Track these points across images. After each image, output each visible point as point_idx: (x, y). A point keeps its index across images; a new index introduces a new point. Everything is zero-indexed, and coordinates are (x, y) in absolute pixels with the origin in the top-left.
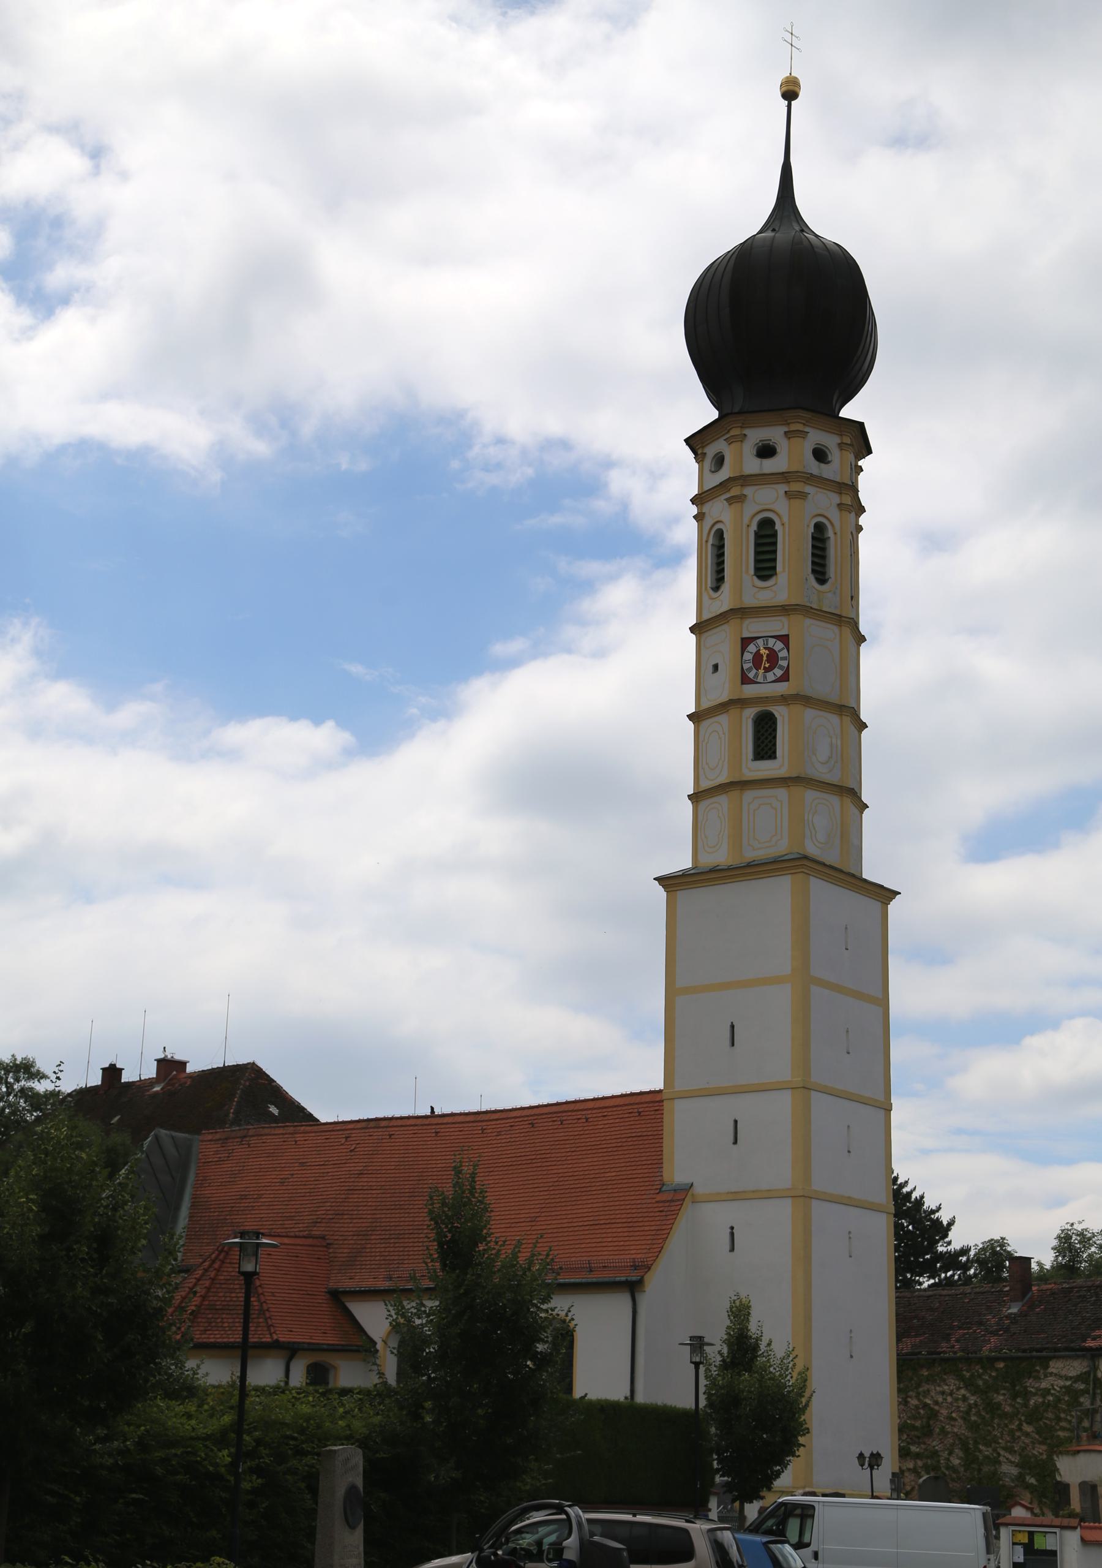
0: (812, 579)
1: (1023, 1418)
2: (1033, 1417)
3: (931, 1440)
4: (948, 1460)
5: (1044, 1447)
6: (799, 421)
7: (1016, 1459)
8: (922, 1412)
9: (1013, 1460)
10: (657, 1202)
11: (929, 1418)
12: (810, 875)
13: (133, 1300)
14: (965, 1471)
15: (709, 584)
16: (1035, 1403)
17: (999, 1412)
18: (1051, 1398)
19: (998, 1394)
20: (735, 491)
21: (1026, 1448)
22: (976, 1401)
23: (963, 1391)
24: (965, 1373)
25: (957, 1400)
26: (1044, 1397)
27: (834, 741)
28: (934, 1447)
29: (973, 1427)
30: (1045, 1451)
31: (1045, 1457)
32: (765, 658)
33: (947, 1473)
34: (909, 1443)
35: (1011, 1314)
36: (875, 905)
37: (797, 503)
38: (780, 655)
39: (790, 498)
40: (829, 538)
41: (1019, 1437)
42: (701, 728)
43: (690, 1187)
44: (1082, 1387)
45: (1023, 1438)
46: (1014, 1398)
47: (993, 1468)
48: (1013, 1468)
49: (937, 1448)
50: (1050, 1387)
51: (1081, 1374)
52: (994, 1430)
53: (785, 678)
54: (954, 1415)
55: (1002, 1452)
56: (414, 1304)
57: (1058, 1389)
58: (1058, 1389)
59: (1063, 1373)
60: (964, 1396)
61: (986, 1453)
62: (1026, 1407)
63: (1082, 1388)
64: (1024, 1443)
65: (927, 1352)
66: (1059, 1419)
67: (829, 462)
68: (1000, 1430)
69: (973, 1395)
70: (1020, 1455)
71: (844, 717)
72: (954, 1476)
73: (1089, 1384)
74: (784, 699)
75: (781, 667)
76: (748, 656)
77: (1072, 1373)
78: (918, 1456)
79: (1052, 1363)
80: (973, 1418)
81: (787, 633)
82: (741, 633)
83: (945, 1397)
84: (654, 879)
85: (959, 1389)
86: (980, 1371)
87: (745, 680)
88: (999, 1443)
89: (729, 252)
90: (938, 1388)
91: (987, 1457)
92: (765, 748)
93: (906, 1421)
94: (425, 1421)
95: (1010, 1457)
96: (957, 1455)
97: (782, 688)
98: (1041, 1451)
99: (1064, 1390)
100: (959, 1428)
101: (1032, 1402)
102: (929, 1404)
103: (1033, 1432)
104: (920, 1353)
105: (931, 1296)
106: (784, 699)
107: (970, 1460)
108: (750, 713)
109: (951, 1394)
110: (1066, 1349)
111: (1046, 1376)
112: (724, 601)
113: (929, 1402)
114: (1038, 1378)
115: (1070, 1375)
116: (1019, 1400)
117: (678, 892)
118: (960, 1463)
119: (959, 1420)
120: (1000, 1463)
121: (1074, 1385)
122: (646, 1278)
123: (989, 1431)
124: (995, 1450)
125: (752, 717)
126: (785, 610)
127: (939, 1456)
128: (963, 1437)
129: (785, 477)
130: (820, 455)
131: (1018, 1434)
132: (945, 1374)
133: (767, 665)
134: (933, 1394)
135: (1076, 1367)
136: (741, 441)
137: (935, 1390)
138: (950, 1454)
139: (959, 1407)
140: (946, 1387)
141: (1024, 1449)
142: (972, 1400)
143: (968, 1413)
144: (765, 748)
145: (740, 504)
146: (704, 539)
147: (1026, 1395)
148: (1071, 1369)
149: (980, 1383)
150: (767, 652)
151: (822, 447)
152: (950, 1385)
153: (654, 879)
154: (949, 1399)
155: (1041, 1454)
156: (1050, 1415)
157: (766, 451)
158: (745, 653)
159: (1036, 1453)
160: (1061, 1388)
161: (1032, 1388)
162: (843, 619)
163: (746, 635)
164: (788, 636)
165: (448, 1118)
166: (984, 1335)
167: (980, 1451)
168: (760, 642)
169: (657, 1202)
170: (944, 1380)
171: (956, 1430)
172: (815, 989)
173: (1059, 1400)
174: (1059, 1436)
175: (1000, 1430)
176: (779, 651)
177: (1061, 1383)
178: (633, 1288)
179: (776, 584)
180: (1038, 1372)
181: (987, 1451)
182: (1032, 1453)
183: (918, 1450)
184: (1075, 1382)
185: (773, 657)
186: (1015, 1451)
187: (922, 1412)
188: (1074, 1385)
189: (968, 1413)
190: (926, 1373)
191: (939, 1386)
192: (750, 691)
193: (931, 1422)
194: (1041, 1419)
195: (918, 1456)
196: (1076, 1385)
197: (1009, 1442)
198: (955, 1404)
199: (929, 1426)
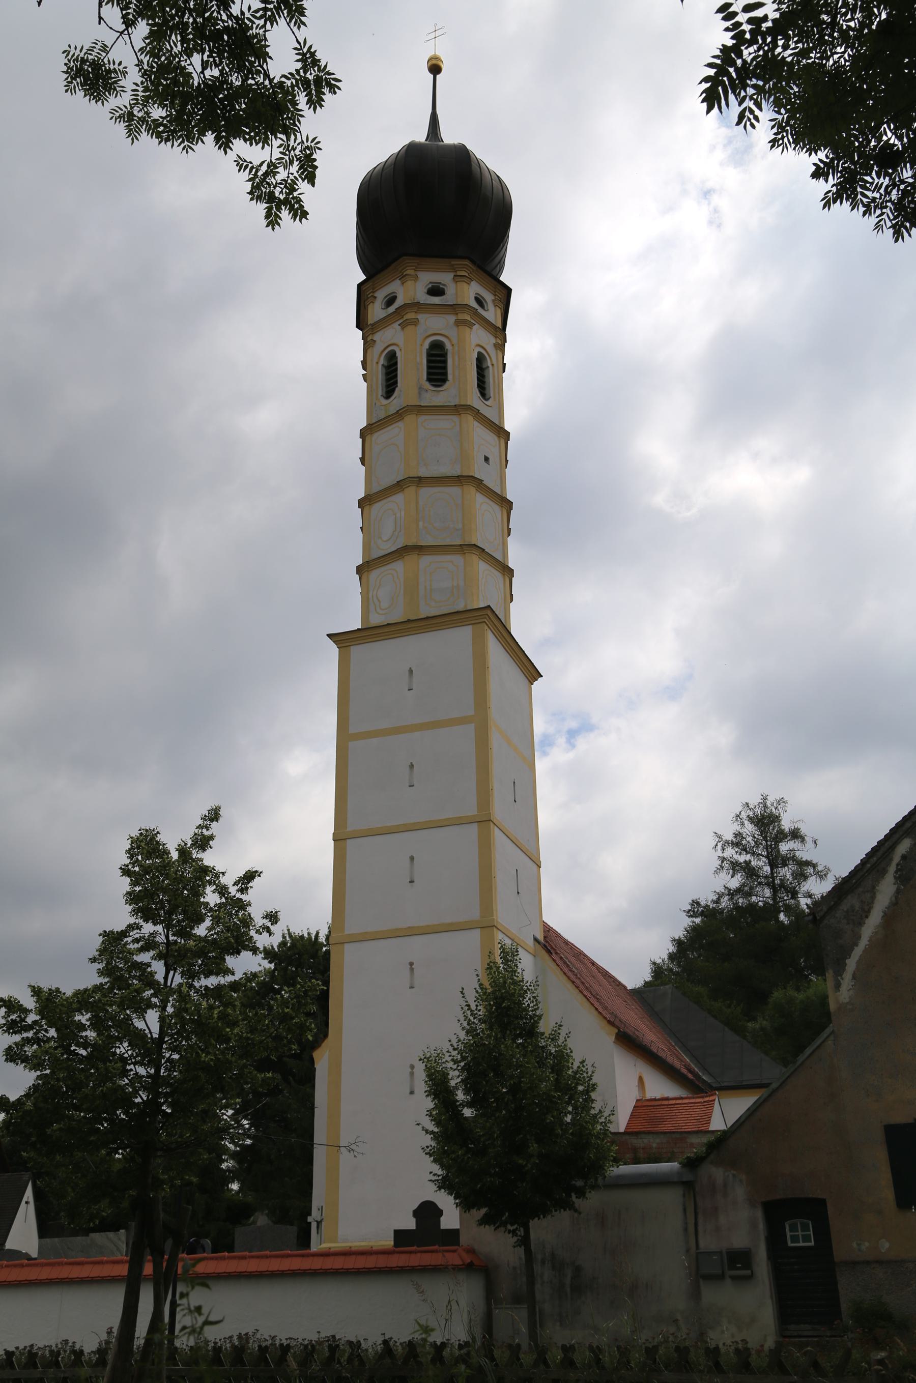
13: (88, 64)
15: (380, 393)
20: (410, 316)
37: (410, 328)
56: (550, 1048)
89: (375, 168)
94: (662, 1340)
112: (395, 403)
117: (352, 647)
130: (479, 301)
145: (413, 326)
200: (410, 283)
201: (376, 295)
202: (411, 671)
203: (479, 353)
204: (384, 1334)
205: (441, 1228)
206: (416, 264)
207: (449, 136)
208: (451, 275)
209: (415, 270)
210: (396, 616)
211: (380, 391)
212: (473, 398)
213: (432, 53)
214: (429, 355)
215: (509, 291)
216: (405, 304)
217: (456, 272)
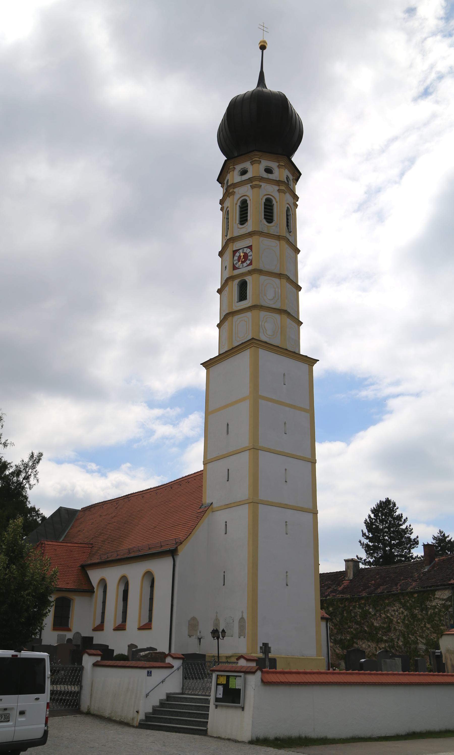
0: (264, 221)
1: (426, 621)
2: (430, 620)
3: (391, 633)
4: (397, 643)
5: (435, 635)
6: (256, 157)
7: (424, 641)
8: (386, 620)
9: (423, 642)
10: (197, 513)
11: (389, 623)
12: (259, 348)
14: (404, 648)
16: (430, 613)
17: (416, 618)
18: (437, 610)
19: (416, 609)
21: (428, 636)
22: (407, 614)
23: (402, 609)
24: (402, 600)
25: (400, 613)
26: (434, 610)
27: (277, 290)
28: (392, 637)
29: (407, 626)
30: (436, 637)
31: (436, 640)
32: (242, 257)
33: (398, 649)
34: (382, 635)
35: (425, 571)
36: (305, 367)
37: (256, 190)
38: (249, 254)
39: (253, 188)
40: (274, 204)
41: (425, 630)
42: (222, 295)
43: (211, 505)
44: (450, 603)
45: (426, 631)
46: (422, 611)
47: (415, 646)
48: (423, 646)
49: (393, 637)
50: (436, 605)
51: (449, 597)
52: (415, 627)
53: (251, 264)
54: (399, 621)
55: (419, 638)
57: (440, 605)
58: (440, 605)
59: (441, 597)
60: (402, 611)
61: (412, 639)
62: (427, 616)
63: (449, 604)
64: (427, 633)
65: (387, 591)
66: (441, 620)
67: (273, 173)
68: (417, 627)
69: (406, 611)
70: (426, 639)
71: (281, 279)
72: (400, 650)
73: (452, 602)
74: (250, 273)
75: (249, 260)
76: (236, 258)
77: (445, 597)
78: (386, 641)
79: (436, 593)
80: (406, 622)
81: (251, 245)
82: (233, 248)
83: (395, 612)
84: (201, 364)
85: (400, 608)
86: (408, 599)
87: (235, 268)
88: (417, 634)
90: (392, 608)
91: (412, 641)
92: (243, 296)
93: (381, 625)
95: (422, 640)
96: (401, 640)
97: (250, 268)
98: (434, 636)
99: (442, 606)
100: (401, 627)
101: (429, 613)
102: (389, 616)
103: (430, 627)
104: (384, 592)
105: (397, 567)
106: (250, 273)
107: (406, 643)
108: (236, 282)
109: (397, 611)
110: (441, 585)
111: (434, 600)
112: (228, 237)
113: (389, 615)
114: (431, 601)
115: (444, 598)
116: (424, 612)
117: (210, 368)
118: (402, 644)
119: (401, 623)
120: (418, 643)
121: (446, 603)
122: (179, 548)
123: (413, 628)
124: (416, 637)
125: (237, 283)
126: (250, 234)
127: (394, 641)
128: (403, 631)
129: (250, 180)
131: (424, 629)
132: (394, 602)
133: (243, 260)
134: (390, 611)
135: (446, 594)
136: (233, 171)
137: (391, 609)
138: (398, 640)
139: (400, 617)
140: (395, 608)
141: (427, 636)
142: (406, 613)
143: (404, 619)
144: (243, 296)
146: (224, 217)
147: (427, 609)
148: (445, 595)
149: (408, 605)
150: (243, 254)
151: (269, 168)
152: (397, 607)
153: (201, 364)
154: (397, 613)
155: (434, 638)
156: (437, 619)
157: (244, 172)
158: (235, 257)
159: (432, 638)
160: (441, 605)
161: (429, 605)
162: (280, 237)
163: (235, 249)
164: (252, 246)
165: (144, 492)
166: (411, 582)
167: (410, 638)
168: (241, 251)
169: (197, 513)
170: (394, 605)
171: (400, 628)
172: (261, 402)
173: (440, 611)
174: (441, 629)
175: (417, 627)
176: (248, 253)
177: (441, 602)
178: (173, 553)
179: (247, 225)
180: (431, 597)
181: (413, 638)
182: (431, 638)
183: (386, 638)
184: (446, 601)
185: (246, 256)
186: (424, 637)
187: (386, 620)
188: (446, 603)
189: (404, 619)
190: (387, 602)
191: (393, 607)
192: (236, 272)
193: (390, 625)
194: (433, 621)
195: (386, 641)
196: (447, 603)
197: (421, 633)
198: (399, 616)
199: (389, 626)
200: (256, 165)
201: (235, 167)
202: (284, 375)
203: (288, 208)
205: (93, 643)
206: (286, 163)
208: (277, 164)
209: (259, 158)
212: (284, 232)
213: (262, 39)
214: (265, 205)
217: (279, 162)
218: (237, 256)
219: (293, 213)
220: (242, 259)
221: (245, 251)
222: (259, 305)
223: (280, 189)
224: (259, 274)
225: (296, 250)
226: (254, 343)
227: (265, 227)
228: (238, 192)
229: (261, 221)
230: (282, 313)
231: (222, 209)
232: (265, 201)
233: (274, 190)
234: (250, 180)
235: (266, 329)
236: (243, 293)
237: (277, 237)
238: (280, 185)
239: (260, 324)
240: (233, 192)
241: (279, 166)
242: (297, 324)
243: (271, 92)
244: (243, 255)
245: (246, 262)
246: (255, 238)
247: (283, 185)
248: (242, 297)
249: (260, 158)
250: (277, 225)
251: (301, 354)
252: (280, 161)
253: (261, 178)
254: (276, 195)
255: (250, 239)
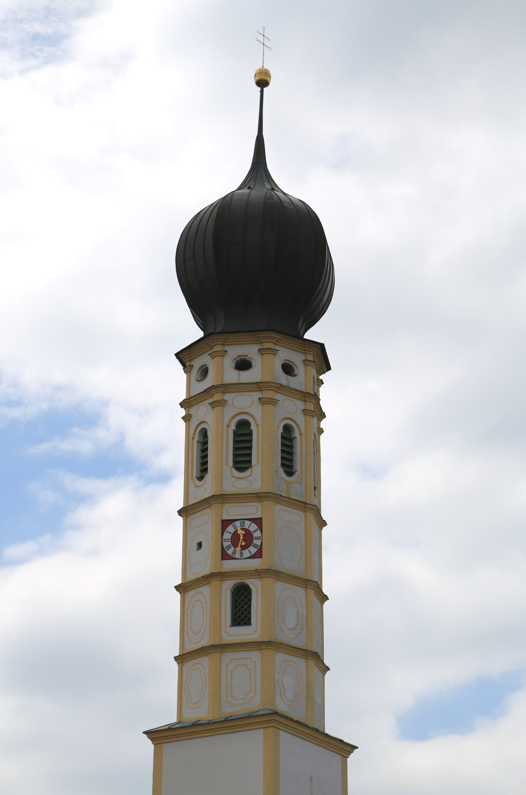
0: (281, 471)
6: (270, 340)
15: (195, 475)
20: (217, 397)
27: (300, 610)
32: (241, 538)
40: (296, 437)
67: (295, 375)
74: (258, 573)
75: (255, 546)
81: (260, 516)
84: (144, 733)
87: (225, 556)
97: (256, 563)
106: (258, 573)
108: (228, 585)
112: (208, 382)
117: (164, 745)
133: (243, 544)
146: (191, 436)
150: (243, 532)
162: (308, 506)
163: (225, 517)
168: (238, 524)
185: (249, 537)
192: (229, 565)
202: (311, 779)
204: (259, 398)
207: (265, 67)
208: (302, 357)
210: (205, 642)
211: (195, 473)
215: (322, 346)
216: (213, 386)
218: (230, 533)
219: (318, 450)
220: (242, 542)
221: (246, 527)
222: (274, 641)
223: (307, 409)
224: (275, 579)
225: (305, 507)
226: (275, 721)
227: (283, 483)
228: (233, 401)
229: (277, 472)
230: (309, 657)
231: (186, 418)
232: (282, 432)
233: (297, 409)
234: (258, 386)
235: (284, 688)
236: (239, 607)
237: (302, 506)
238: (307, 400)
239: (276, 678)
240: (224, 402)
241: (307, 362)
242: (323, 672)
243: (295, 207)
244: (244, 534)
245: (248, 549)
246: (269, 504)
247: (312, 401)
248: (238, 615)
249: (277, 343)
250: (302, 480)
251: (326, 732)
252: (307, 352)
253: (279, 386)
254: (300, 419)
255: (257, 504)
